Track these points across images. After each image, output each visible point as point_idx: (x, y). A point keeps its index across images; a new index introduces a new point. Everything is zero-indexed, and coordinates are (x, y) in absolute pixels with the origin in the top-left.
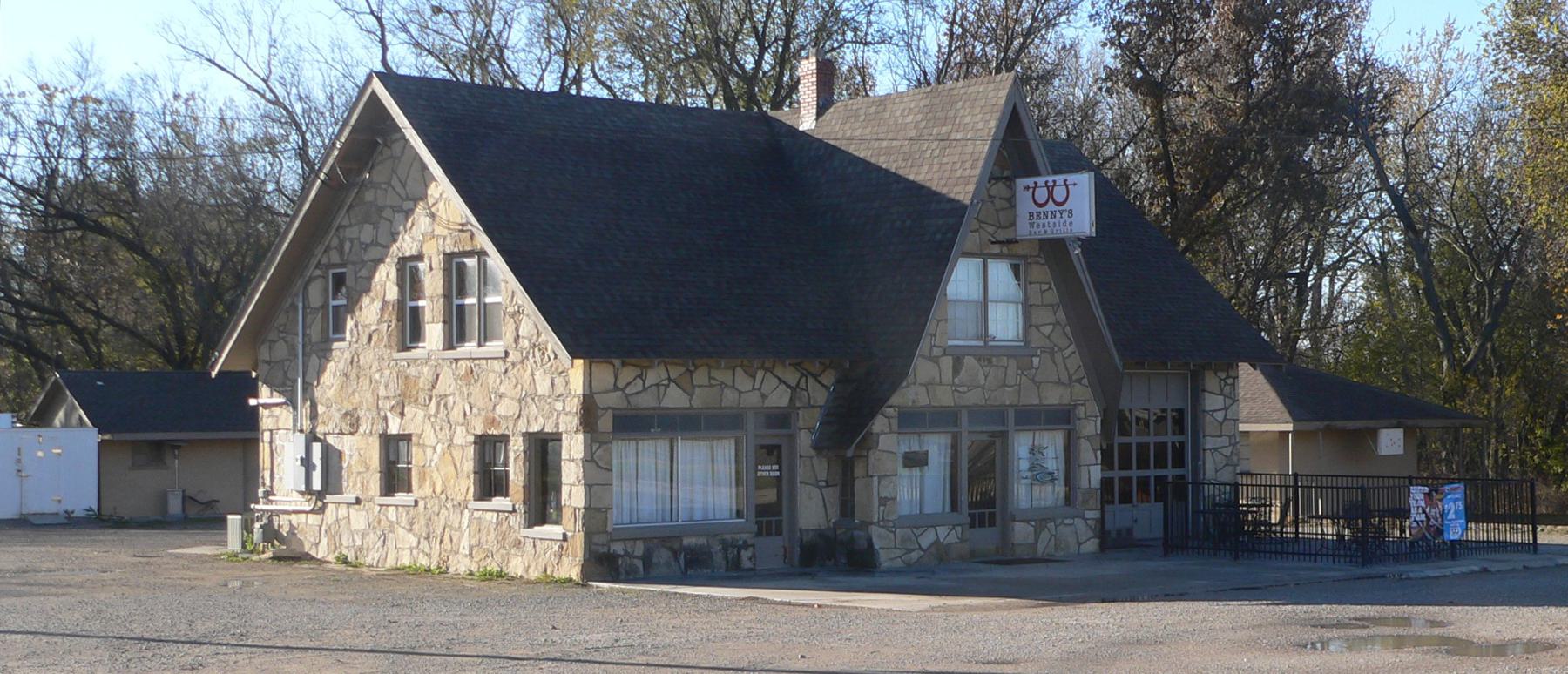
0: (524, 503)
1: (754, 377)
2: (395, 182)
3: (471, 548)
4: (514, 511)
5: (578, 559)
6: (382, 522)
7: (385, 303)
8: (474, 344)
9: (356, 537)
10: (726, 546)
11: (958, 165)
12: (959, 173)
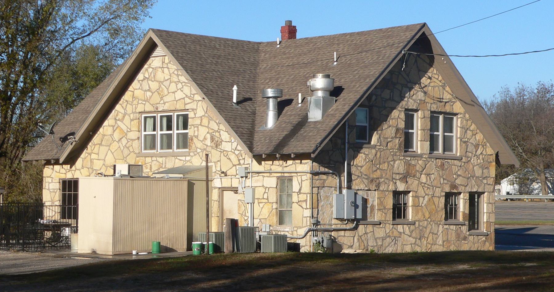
3: (444, 242)
7: (398, 130)
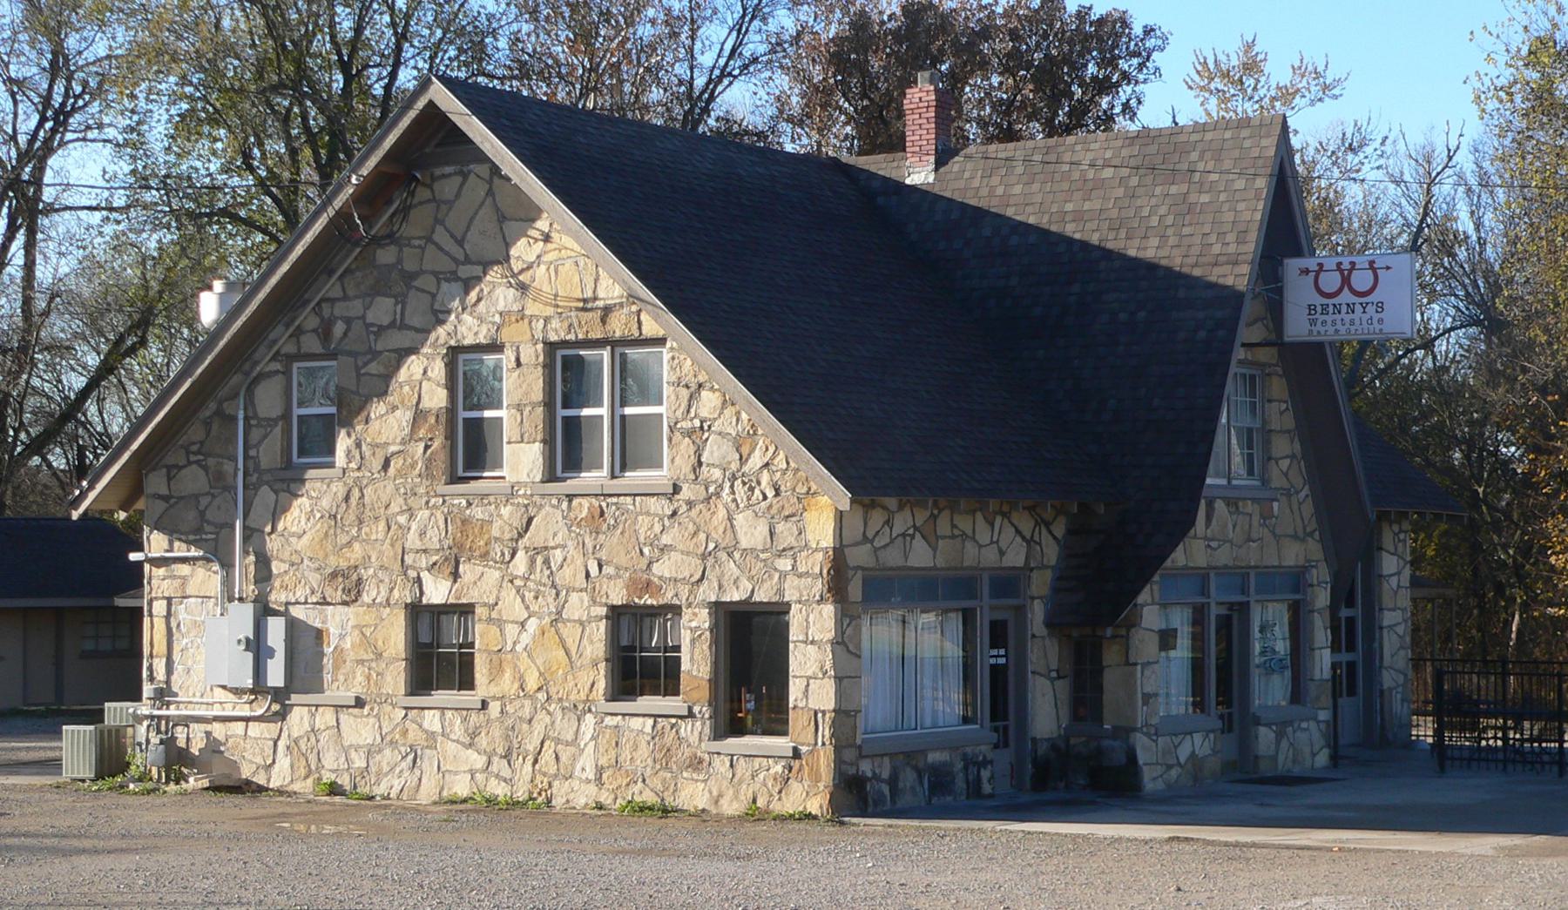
0: (710, 705)
1: (992, 525)
2: (440, 236)
4: (691, 715)
5: (821, 785)
6: (411, 735)
7: (419, 416)
8: (605, 472)
9: (353, 754)
10: (968, 762)
11: (1213, 239)
12: (1217, 249)
